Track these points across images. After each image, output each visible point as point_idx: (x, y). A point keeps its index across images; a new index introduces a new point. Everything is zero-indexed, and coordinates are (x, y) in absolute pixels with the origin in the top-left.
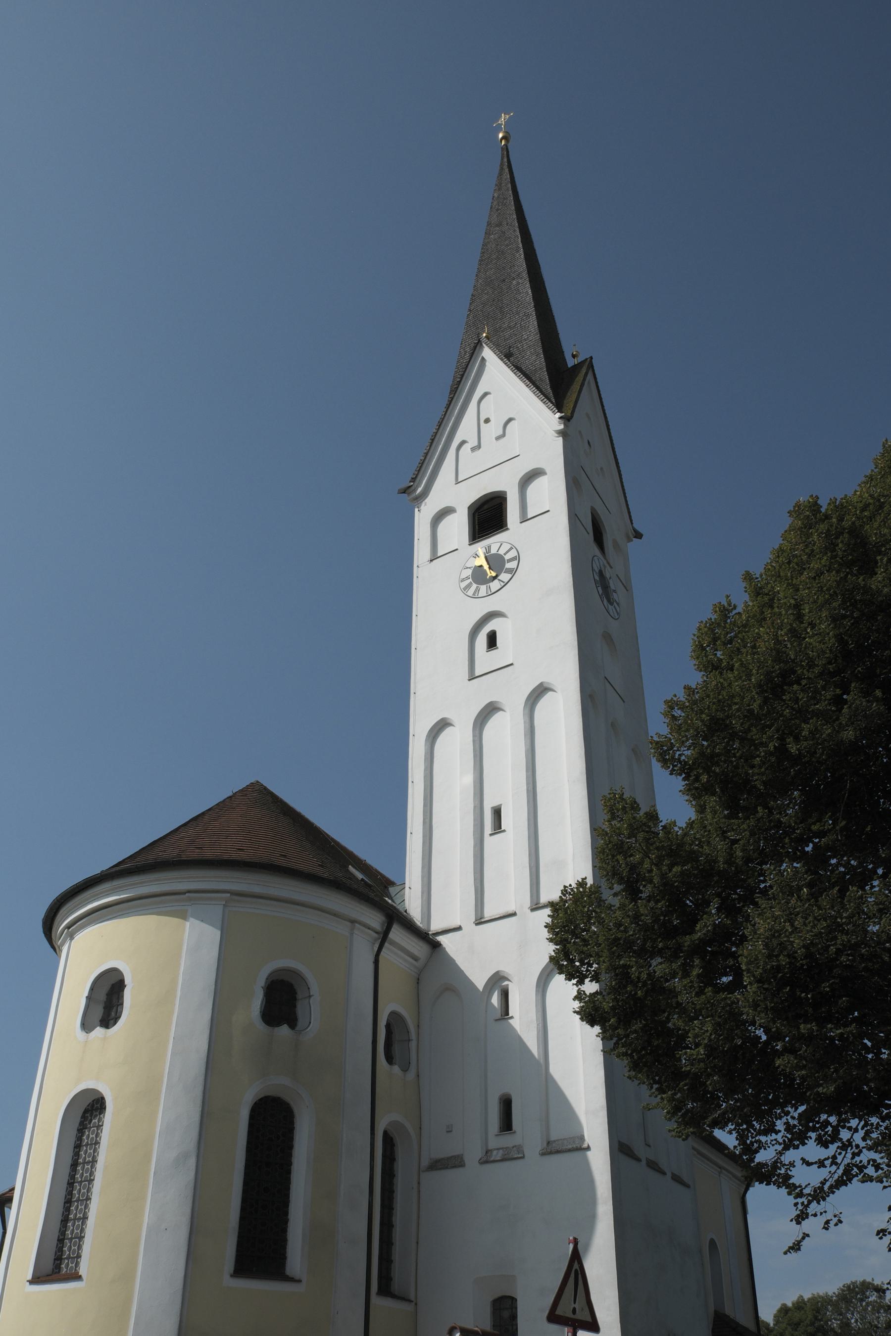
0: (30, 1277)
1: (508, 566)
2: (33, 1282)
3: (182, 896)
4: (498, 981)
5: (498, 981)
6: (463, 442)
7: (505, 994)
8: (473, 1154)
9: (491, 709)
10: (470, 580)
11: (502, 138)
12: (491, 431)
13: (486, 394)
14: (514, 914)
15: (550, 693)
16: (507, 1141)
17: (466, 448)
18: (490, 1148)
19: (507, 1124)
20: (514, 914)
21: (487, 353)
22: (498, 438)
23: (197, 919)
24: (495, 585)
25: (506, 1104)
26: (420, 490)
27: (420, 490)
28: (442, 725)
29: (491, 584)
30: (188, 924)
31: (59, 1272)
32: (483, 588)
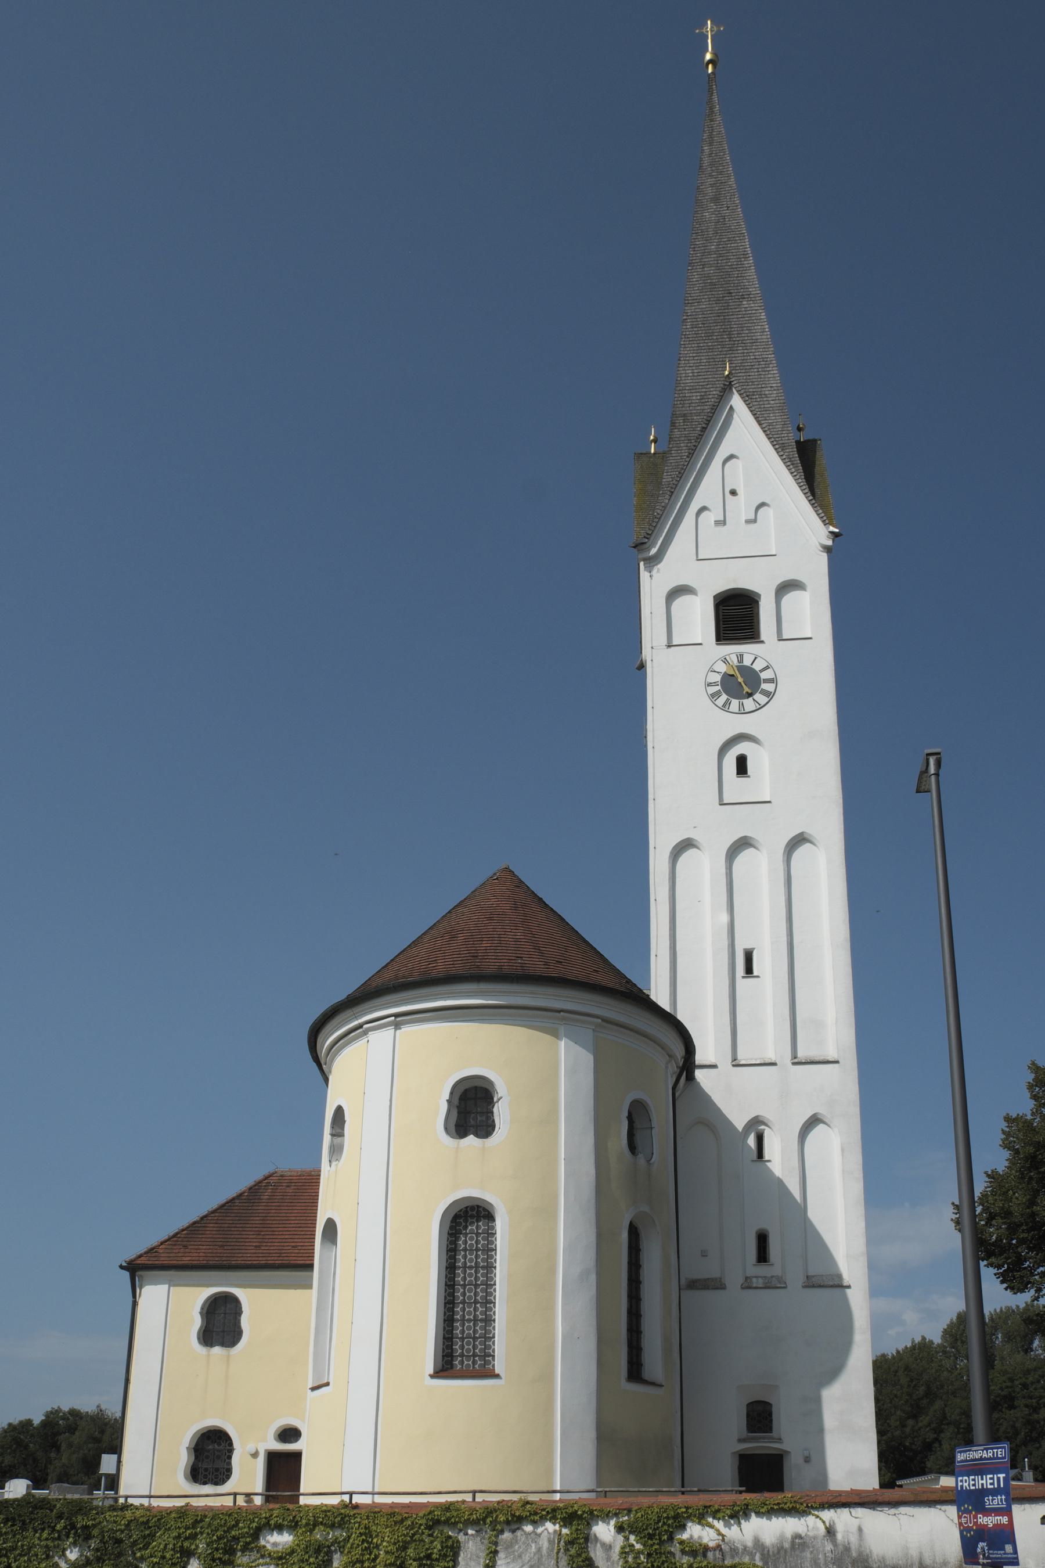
0: (432, 1372)
1: (764, 686)
2: (432, 1376)
3: (557, 1014)
4: (756, 1125)
5: (756, 1125)
6: (704, 509)
7: (760, 1139)
8: (734, 1279)
9: (743, 844)
10: (719, 688)
11: (710, 61)
12: (741, 508)
13: (732, 457)
14: (774, 1064)
15: (808, 845)
16: (763, 1270)
17: (708, 519)
18: (748, 1275)
19: (763, 1256)
20: (774, 1064)
21: (736, 401)
22: (748, 522)
23: (571, 1039)
24: (749, 704)
25: (762, 1239)
26: (654, 551)
27: (654, 551)
28: (686, 845)
29: (745, 701)
30: (562, 1044)
31: (452, 1368)
32: (735, 703)
